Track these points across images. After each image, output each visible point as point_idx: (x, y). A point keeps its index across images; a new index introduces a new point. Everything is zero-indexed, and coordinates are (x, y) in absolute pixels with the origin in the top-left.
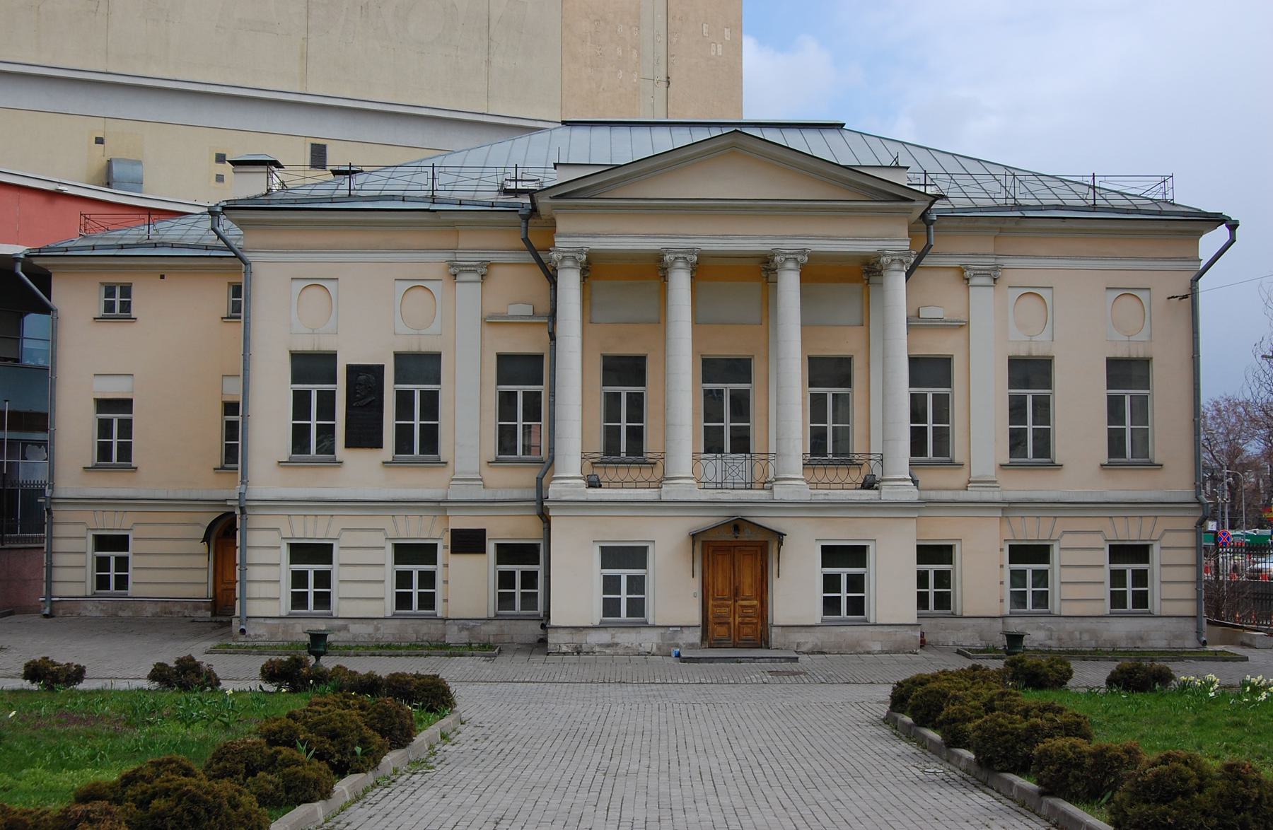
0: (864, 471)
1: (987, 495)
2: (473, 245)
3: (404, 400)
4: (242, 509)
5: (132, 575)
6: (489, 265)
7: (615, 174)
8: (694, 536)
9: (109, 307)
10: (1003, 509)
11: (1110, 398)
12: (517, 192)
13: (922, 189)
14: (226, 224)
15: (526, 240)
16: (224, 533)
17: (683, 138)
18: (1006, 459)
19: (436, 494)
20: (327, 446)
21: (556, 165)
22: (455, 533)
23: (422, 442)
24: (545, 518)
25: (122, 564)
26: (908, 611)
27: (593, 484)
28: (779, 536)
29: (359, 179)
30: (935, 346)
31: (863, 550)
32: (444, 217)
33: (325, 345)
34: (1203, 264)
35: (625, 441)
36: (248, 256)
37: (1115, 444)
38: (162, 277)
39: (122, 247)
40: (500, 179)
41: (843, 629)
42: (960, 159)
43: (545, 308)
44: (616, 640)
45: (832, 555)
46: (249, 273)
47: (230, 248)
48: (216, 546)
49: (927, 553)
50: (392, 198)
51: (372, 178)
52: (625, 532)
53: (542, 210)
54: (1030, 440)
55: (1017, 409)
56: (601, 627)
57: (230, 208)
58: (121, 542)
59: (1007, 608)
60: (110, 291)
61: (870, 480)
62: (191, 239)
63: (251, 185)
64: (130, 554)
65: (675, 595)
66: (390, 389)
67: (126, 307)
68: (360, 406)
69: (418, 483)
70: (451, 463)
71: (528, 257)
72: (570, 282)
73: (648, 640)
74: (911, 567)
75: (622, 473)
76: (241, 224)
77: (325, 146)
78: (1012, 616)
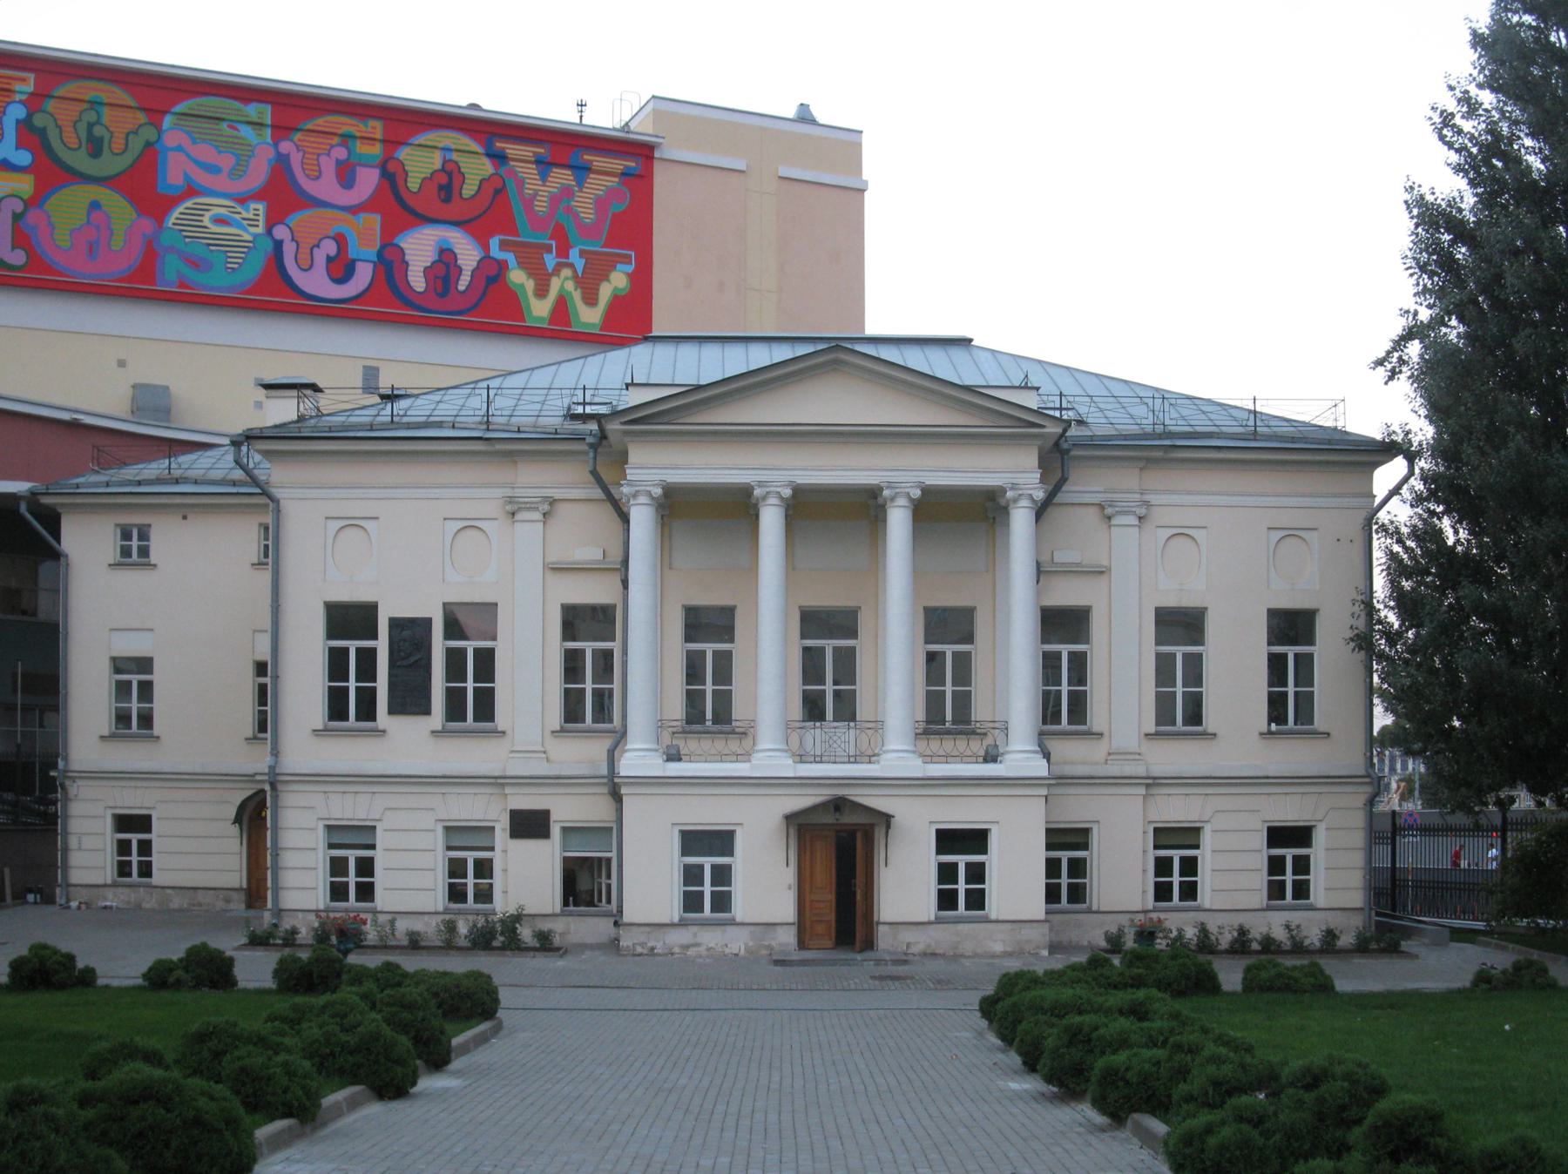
0: (989, 741)
1: (1128, 770)
2: (535, 479)
3: (455, 661)
4: (273, 786)
5: (156, 859)
6: (553, 502)
7: (699, 396)
8: (790, 818)
9: (126, 552)
10: (1148, 785)
11: (1159, 656)
12: (585, 418)
13: (1057, 414)
14: (255, 459)
15: (594, 473)
16: (254, 816)
17: (783, 353)
18: (1152, 728)
19: (492, 768)
20: (367, 710)
21: (627, 386)
22: (515, 815)
23: (475, 706)
24: (617, 797)
25: (145, 848)
26: (1035, 905)
27: (673, 756)
28: (887, 819)
29: (402, 404)
30: (1065, 595)
31: (730, 835)
32: (499, 447)
33: (362, 595)
34: (1377, 501)
35: (708, 709)
36: (275, 492)
37: (1276, 707)
38: (185, 518)
39: (139, 483)
40: (566, 402)
41: (960, 927)
42: (1051, 370)
43: (616, 556)
44: (699, 940)
45: (949, 840)
46: (278, 512)
47: (255, 481)
48: (250, 829)
49: (1165, 836)
50: (440, 425)
51: (419, 402)
52: (708, 813)
53: (612, 438)
54: (1181, 710)
55: (1164, 668)
56: (682, 924)
57: (250, 437)
58: (142, 823)
59: (1150, 902)
60: (126, 535)
61: (993, 752)
62: (216, 474)
63: (283, 410)
64: (153, 836)
65: (766, 887)
66: (439, 646)
67: (144, 551)
68: (399, 665)
69: (471, 755)
70: (509, 732)
71: (598, 493)
72: (642, 518)
73: (736, 942)
74: (1038, 855)
75: (706, 744)
76: (267, 454)
77: (377, 369)
78: (1155, 910)
